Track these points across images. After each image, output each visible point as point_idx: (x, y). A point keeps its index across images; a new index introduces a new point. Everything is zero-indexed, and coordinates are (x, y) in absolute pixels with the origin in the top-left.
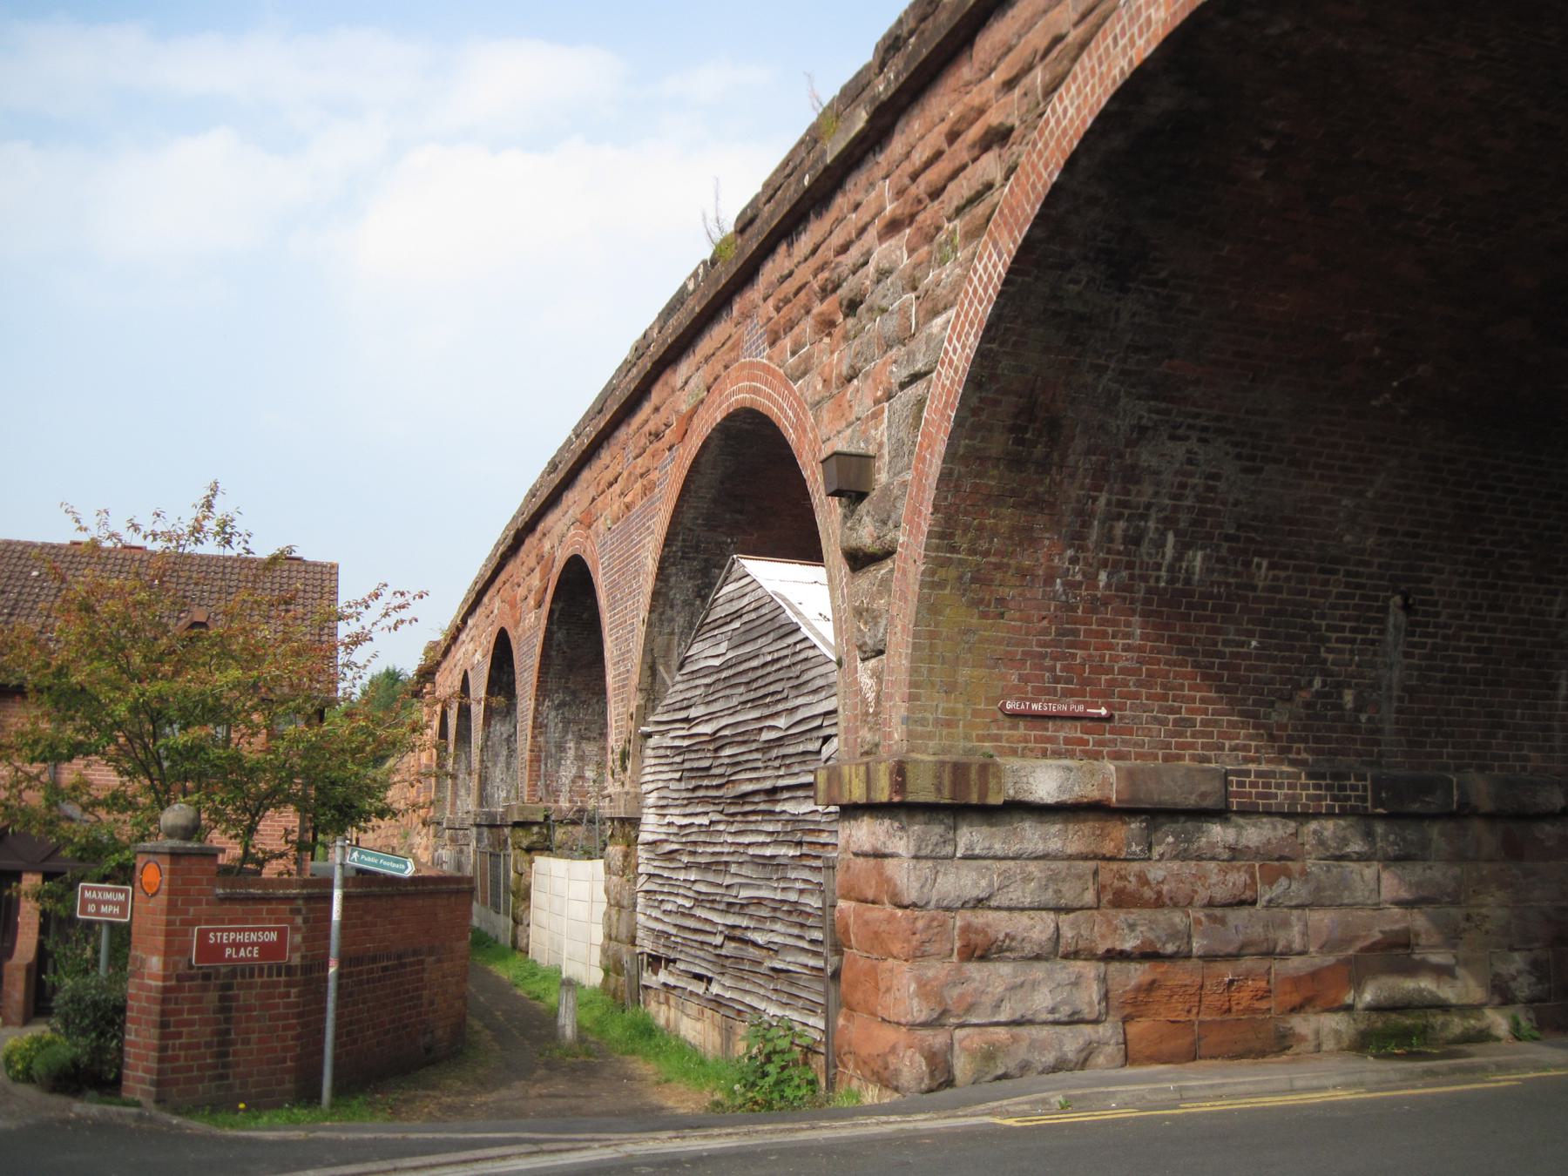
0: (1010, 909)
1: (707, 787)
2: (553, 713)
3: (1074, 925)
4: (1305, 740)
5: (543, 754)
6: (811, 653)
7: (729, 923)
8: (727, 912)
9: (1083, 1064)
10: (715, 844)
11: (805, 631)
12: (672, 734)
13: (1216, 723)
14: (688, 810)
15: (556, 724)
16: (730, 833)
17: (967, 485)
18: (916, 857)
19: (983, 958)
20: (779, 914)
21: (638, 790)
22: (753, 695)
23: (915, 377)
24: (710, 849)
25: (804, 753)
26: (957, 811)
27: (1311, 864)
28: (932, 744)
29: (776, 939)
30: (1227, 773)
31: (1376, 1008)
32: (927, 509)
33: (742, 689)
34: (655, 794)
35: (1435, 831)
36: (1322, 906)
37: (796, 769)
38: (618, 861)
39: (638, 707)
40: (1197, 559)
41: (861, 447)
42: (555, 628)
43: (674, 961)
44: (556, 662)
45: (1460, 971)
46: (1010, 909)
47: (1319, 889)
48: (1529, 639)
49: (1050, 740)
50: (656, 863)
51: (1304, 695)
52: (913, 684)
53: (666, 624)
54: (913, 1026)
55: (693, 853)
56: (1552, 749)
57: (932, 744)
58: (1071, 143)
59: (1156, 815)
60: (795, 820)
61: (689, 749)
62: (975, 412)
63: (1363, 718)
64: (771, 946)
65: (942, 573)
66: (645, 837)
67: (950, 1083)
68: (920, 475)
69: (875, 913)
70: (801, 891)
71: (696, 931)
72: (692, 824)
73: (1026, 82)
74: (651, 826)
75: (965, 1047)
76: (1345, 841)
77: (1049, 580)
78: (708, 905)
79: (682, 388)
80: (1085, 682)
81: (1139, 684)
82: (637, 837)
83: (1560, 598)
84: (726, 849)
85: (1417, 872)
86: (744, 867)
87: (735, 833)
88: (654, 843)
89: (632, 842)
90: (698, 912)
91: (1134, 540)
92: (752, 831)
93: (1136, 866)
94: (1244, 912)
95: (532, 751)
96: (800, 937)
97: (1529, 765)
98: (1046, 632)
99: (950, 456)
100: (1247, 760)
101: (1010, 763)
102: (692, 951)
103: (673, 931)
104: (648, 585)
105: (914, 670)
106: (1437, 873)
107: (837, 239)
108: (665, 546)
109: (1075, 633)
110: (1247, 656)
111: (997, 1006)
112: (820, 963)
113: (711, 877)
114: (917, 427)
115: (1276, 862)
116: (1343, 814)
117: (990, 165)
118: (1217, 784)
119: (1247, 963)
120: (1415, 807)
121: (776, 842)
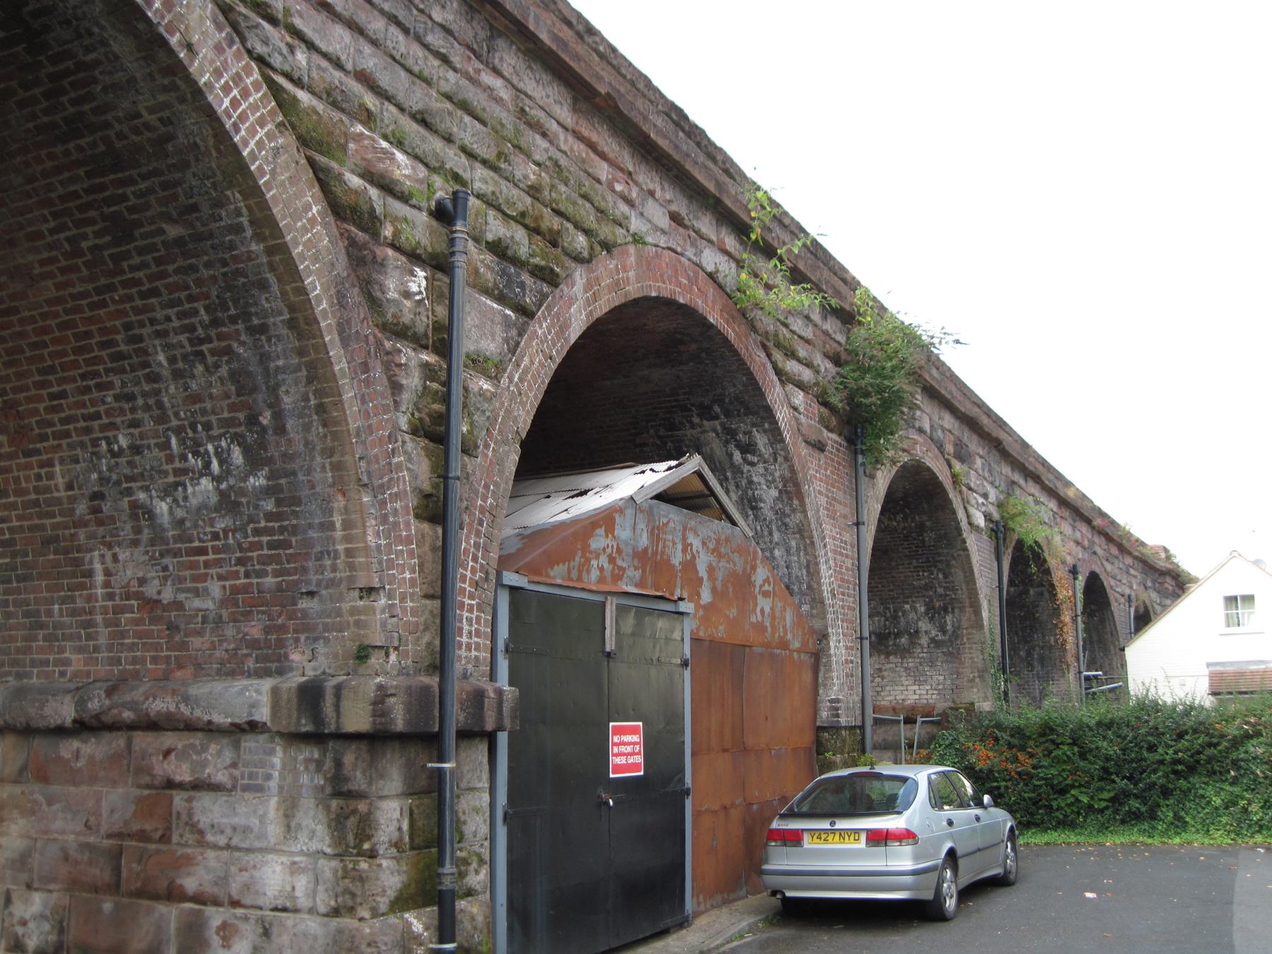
48: (47, 522)
56: (96, 649)
83: (58, 468)
97: (70, 670)
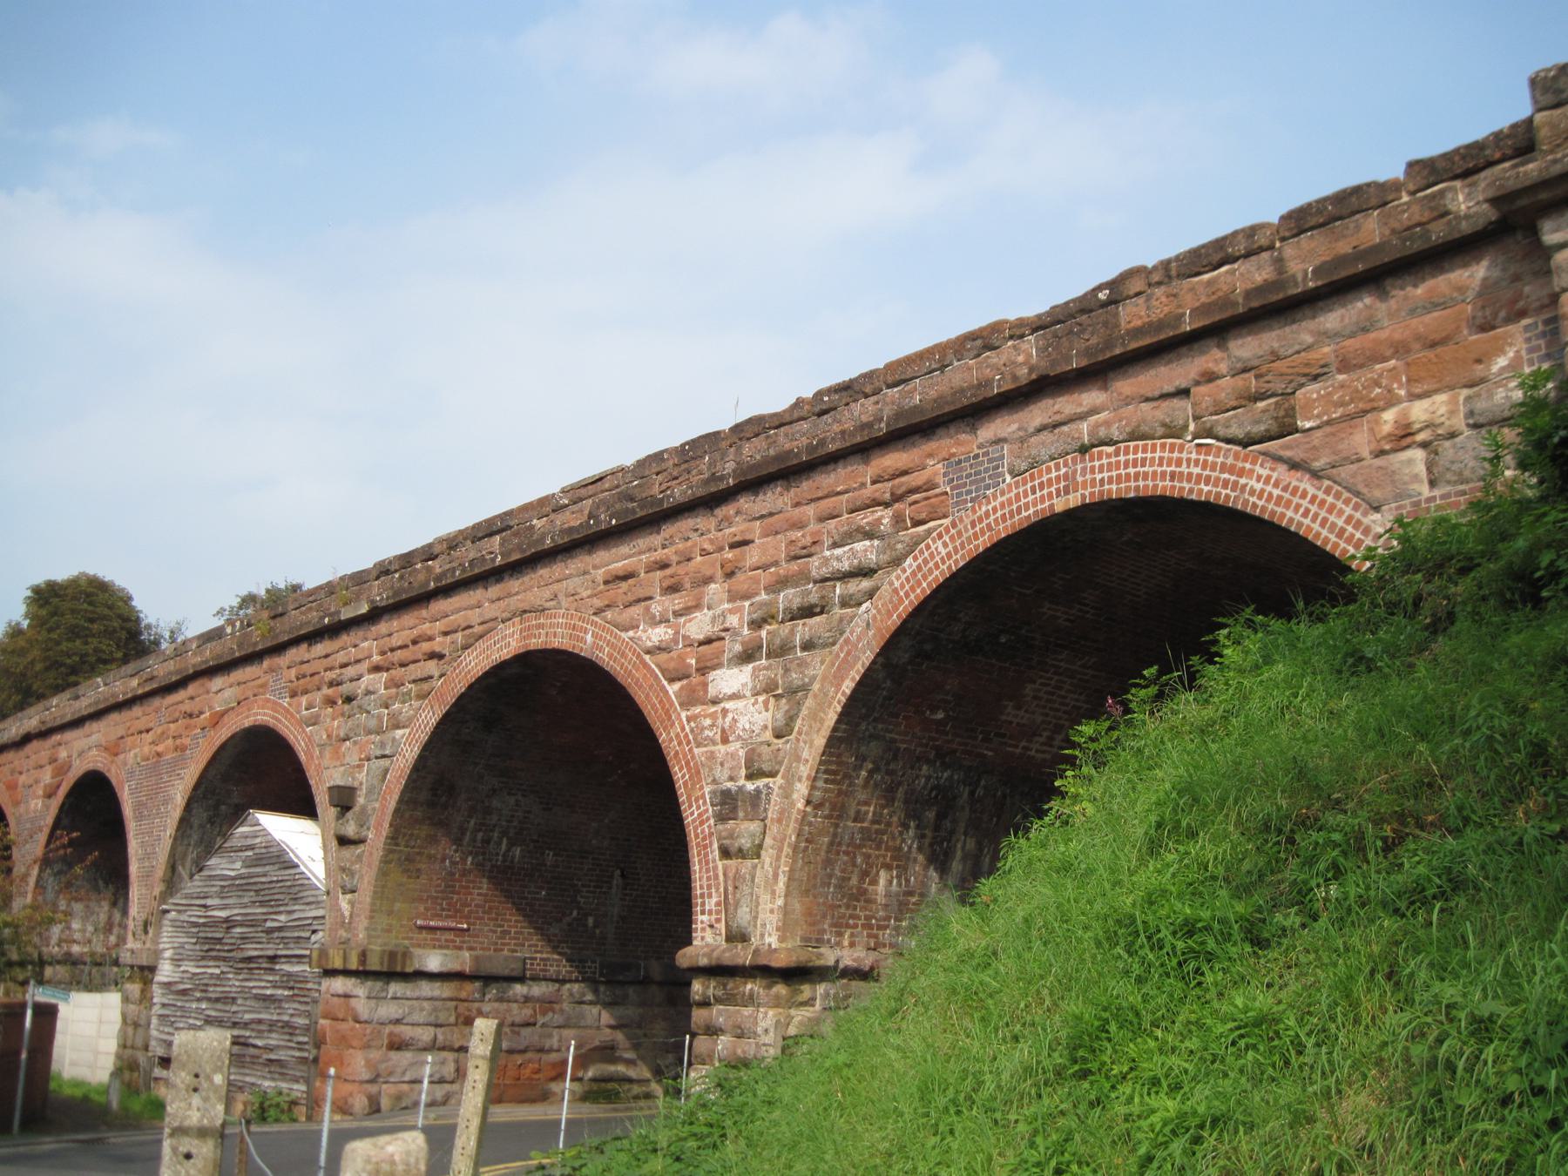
0: (413, 1025)
2: (52, 879)
3: (443, 1033)
4: (567, 942)
6: (306, 882)
9: (444, 1103)
11: (302, 867)
13: (521, 933)
17: (407, 815)
18: (369, 998)
19: (399, 1049)
22: (260, 898)
23: (384, 756)
25: (299, 937)
26: (389, 976)
27: (565, 1006)
28: (379, 941)
30: (525, 959)
31: (594, 1080)
32: (386, 825)
33: (252, 893)
35: (631, 990)
36: (569, 1027)
37: (292, 946)
39: (161, 893)
40: (517, 851)
41: (349, 782)
45: (639, 1062)
46: (413, 1025)
47: (569, 1018)
49: (439, 940)
51: (567, 919)
52: (372, 911)
54: (362, 1082)
55: (205, 991)
57: (379, 941)
58: (471, 679)
59: (488, 979)
60: (289, 975)
61: (204, 925)
62: (415, 781)
63: (598, 931)
65: (391, 856)
67: (378, 1110)
68: (383, 807)
69: (343, 1026)
70: (292, 1015)
73: (454, 636)
74: (165, 972)
75: (387, 1091)
76: (584, 995)
77: (443, 860)
79: (217, 693)
80: (457, 911)
81: (484, 912)
85: (620, 1011)
91: (487, 841)
93: (476, 1005)
94: (529, 1029)
96: (289, 1041)
98: (439, 886)
99: (400, 801)
100: (536, 952)
101: (417, 951)
104: (177, 814)
105: (373, 904)
106: (631, 1012)
107: (341, 657)
109: (454, 886)
110: (538, 899)
111: (404, 1073)
112: (305, 1054)
113: (219, 1006)
114: (383, 780)
115: (548, 1003)
116: (583, 981)
117: (432, 667)
118: (520, 965)
119: (529, 1055)
120: (621, 978)
121: (274, 987)
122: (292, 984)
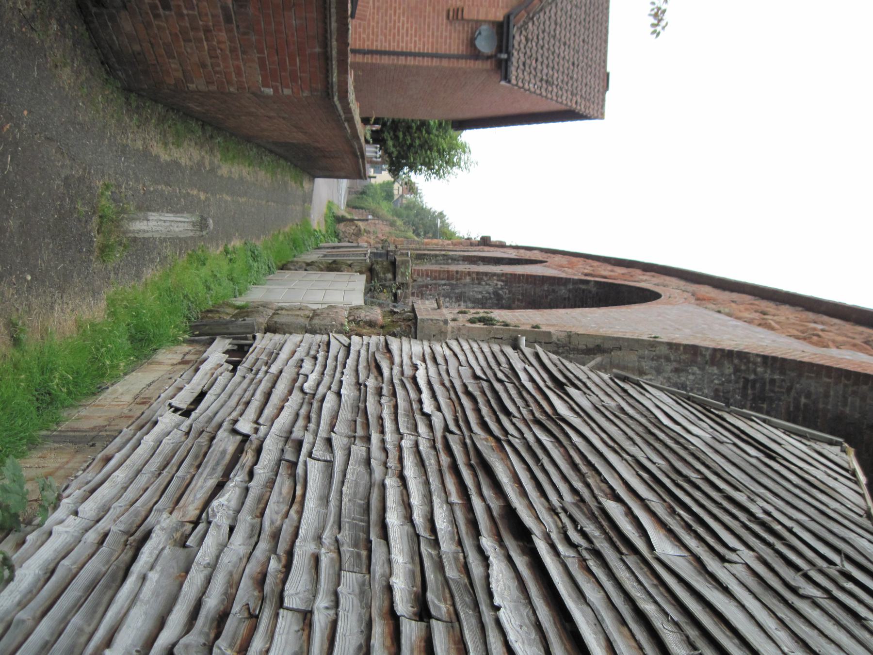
1: (478, 411)
2: (491, 290)
5: (454, 282)
7: (267, 444)
8: (287, 439)
10: (396, 420)
12: (530, 369)
14: (437, 387)
15: (481, 293)
16: (417, 445)
20: (264, 545)
21: (449, 335)
24: (387, 414)
29: (210, 542)
34: (448, 352)
38: (363, 315)
42: (571, 286)
43: (234, 371)
44: (538, 290)
50: (363, 353)
53: (654, 364)
55: (379, 393)
64: (201, 527)
66: (394, 343)
70: (306, 617)
71: (268, 395)
72: (419, 391)
78: (303, 412)
82: (394, 335)
84: (389, 437)
86: (362, 469)
87: (418, 453)
88: (389, 351)
89: (386, 330)
90: (296, 396)
92: (427, 483)
95: (457, 272)
102: (239, 391)
103: (274, 369)
108: (765, 358)
113: (345, 414)
122: (438, 605)
